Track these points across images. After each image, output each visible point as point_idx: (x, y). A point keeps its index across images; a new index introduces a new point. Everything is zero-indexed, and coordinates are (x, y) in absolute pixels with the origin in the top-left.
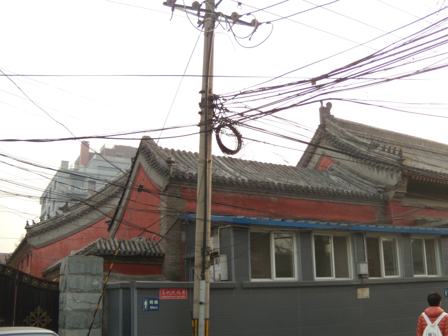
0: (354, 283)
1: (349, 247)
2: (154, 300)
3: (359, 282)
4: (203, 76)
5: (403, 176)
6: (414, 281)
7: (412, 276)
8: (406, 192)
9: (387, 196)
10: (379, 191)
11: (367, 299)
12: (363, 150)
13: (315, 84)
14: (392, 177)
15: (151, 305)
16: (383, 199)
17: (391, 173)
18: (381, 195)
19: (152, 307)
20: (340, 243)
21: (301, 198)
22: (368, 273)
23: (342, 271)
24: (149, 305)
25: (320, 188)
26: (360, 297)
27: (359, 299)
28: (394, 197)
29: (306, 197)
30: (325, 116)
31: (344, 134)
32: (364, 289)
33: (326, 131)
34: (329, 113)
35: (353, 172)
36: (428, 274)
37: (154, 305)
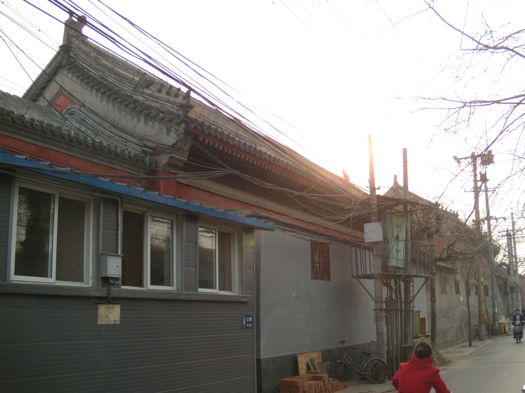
0: (92, 294)
2: (249, 317)
3: (102, 292)
5: (187, 132)
6: (198, 298)
7: (196, 290)
9: (156, 162)
10: (144, 152)
11: (115, 325)
12: (127, 89)
14: (168, 131)
16: (150, 165)
18: (148, 158)
19: (248, 325)
20: (73, 213)
21: (8, 134)
22: (120, 276)
23: (70, 268)
24: (246, 322)
25: (47, 124)
26: (101, 321)
28: (168, 163)
29: (19, 134)
31: (99, 64)
32: (111, 306)
35: (104, 119)
37: (249, 323)
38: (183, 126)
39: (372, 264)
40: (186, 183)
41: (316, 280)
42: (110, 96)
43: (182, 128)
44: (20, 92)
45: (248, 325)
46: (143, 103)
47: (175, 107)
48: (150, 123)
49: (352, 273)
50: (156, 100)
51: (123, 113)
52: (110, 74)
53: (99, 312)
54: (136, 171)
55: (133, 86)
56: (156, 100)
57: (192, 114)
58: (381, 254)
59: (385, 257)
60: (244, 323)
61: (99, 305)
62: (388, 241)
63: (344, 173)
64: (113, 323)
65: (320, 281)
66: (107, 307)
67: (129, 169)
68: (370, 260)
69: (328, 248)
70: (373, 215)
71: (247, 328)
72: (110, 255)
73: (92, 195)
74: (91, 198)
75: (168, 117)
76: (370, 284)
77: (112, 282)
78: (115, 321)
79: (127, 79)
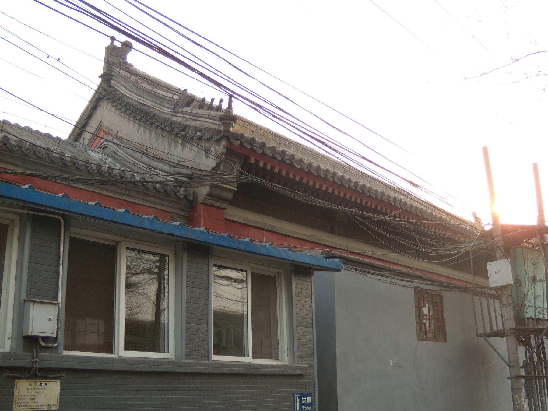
2: (307, 396)
5: (230, 152)
8: (235, 189)
9: (195, 193)
12: (165, 110)
17: (207, 145)
19: (304, 408)
24: (302, 405)
28: (209, 195)
30: (115, 61)
32: (43, 382)
33: (111, 86)
34: (124, 58)
36: (254, 357)
37: (307, 405)
38: (224, 143)
39: (503, 318)
40: (242, 221)
41: (425, 342)
42: (135, 116)
43: (222, 147)
44: (65, 136)
46: (180, 124)
47: (216, 122)
48: (188, 145)
49: (477, 331)
50: (196, 118)
51: (160, 139)
52: (149, 98)
53: (16, 391)
54: (167, 206)
55: (172, 107)
56: (196, 118)
57: (235, 129)
58: (513, 302)
59: (519, 307)
60: (298, 405)
61: (17, 381)
62: (520, 283)
63: (475, 215)
65: (430, 343)
66: (33, 383)
67: (156, 203)
68: (495, 310)
69: (441, 297)
70: (498, 251)
72: (35, 302)
73: (16, 214)
74: (17, 218)
75: (207, 135)
76: (501, 344)
77: (43, 344)
78: (49, 405)
79: (166, 100)
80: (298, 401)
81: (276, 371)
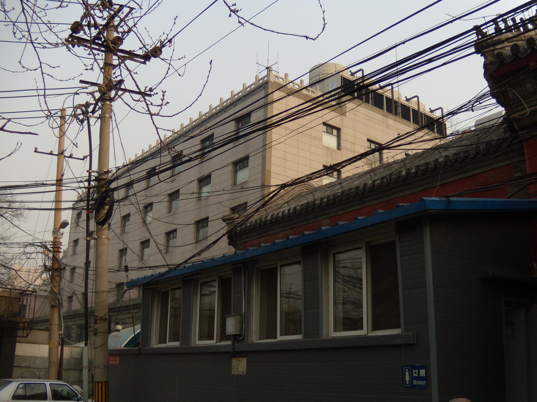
1: (328, 282)
2: (419, 368)
4: (61, 201)
13: (250, 122)
15: (415, 378)
19: (415, 382)
24: (412, 378)
27: (234, 375)
37: (419, 378)
45: (415, 382)
60: (407, 378)
64: (241, 374)
71: (413, 386)
80: (407, 373)
81: (398, 341)
